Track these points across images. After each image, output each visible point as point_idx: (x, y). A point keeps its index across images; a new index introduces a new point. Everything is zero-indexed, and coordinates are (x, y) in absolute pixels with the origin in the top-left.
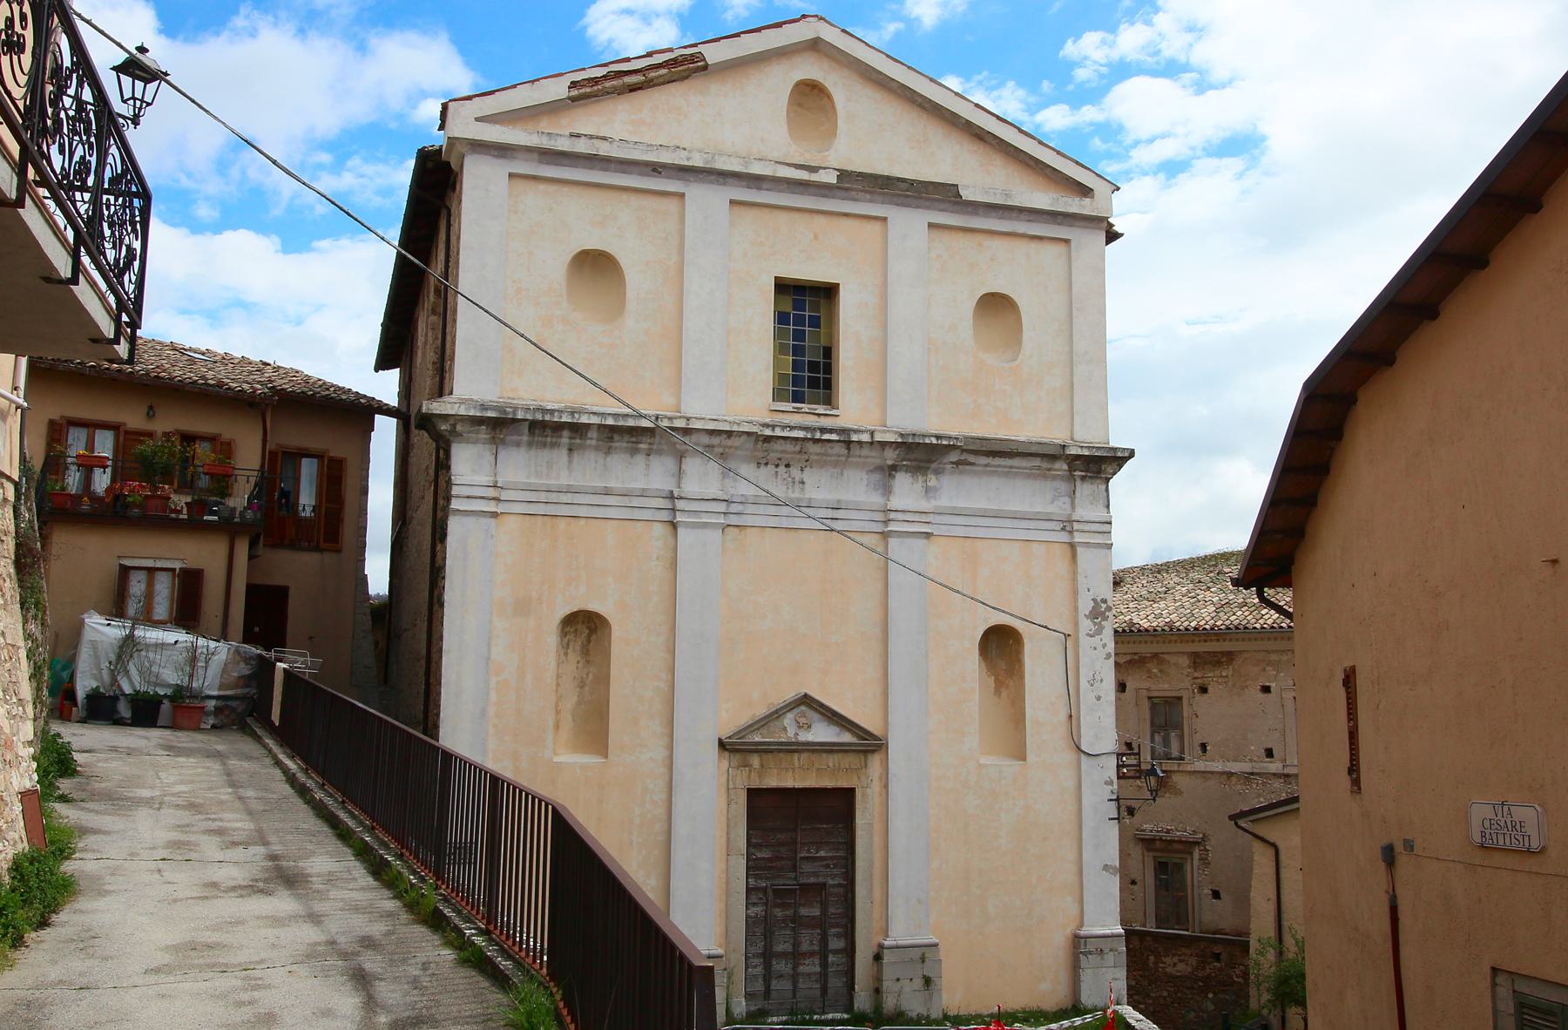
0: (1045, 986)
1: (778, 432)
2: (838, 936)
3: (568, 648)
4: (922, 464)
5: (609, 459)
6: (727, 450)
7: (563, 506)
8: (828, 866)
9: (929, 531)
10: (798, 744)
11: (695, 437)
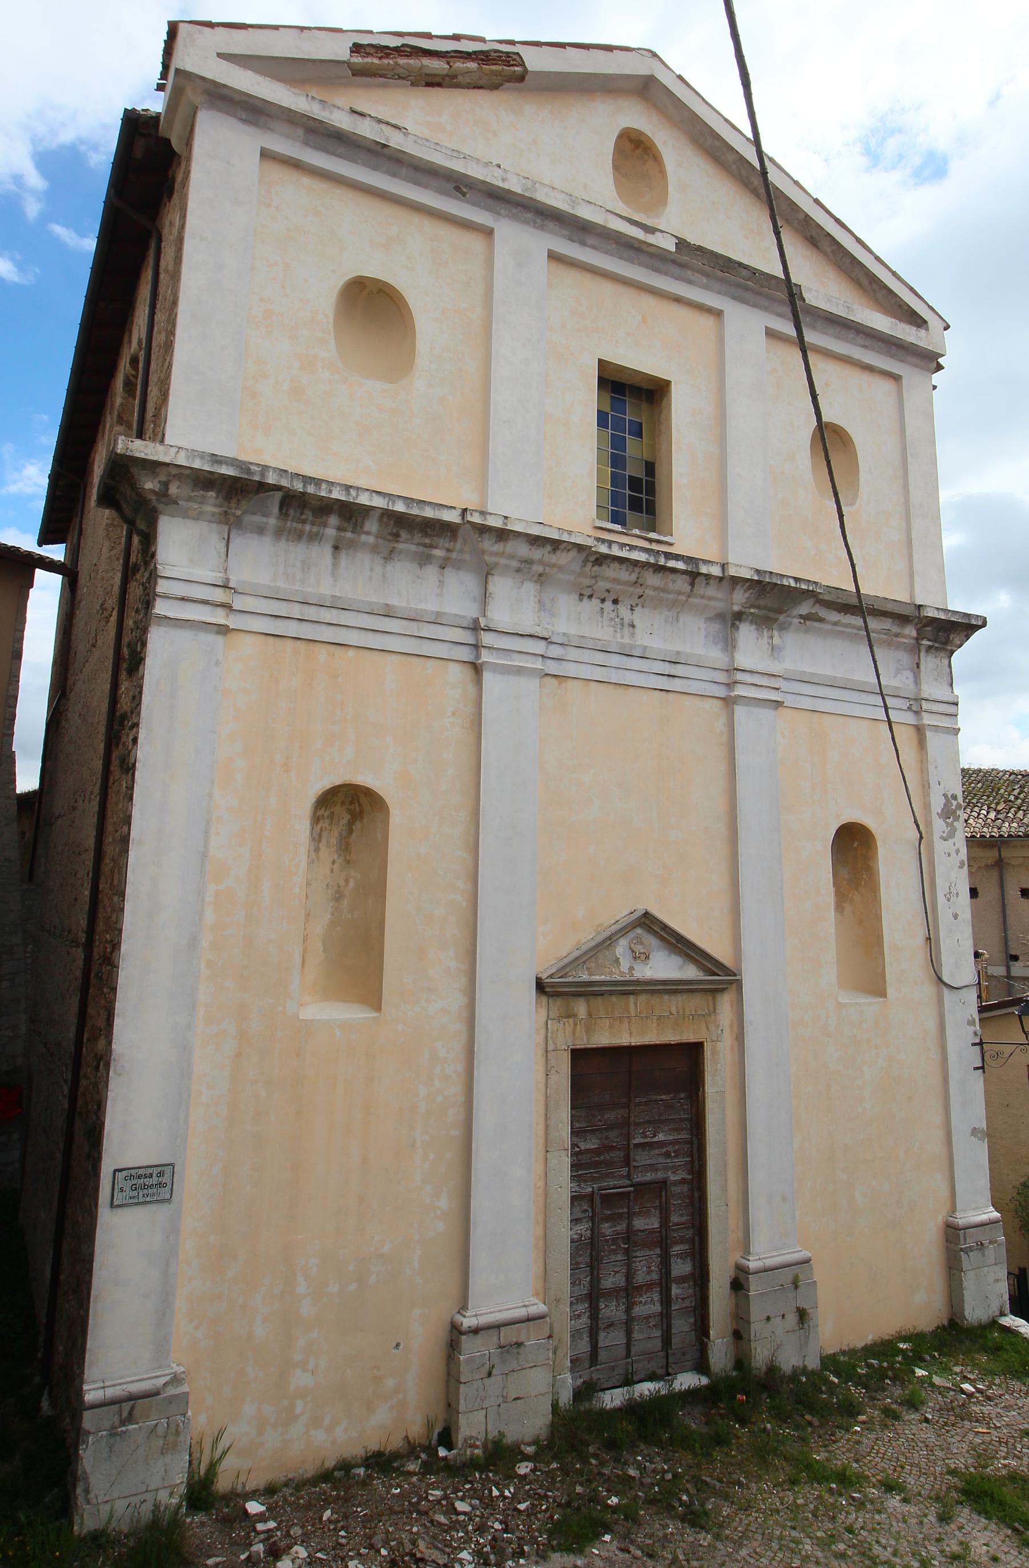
0: (920, 1298)
1: (616, 551)
2: (681, 1256)
3: (320, 841)
4: (771, 615)
5: (389, 567)
6: (548, 569)
7: (325, 627)
8: (667, 1155)
9: (779, 699)
10: (638, 982)
11: (510, 546)
